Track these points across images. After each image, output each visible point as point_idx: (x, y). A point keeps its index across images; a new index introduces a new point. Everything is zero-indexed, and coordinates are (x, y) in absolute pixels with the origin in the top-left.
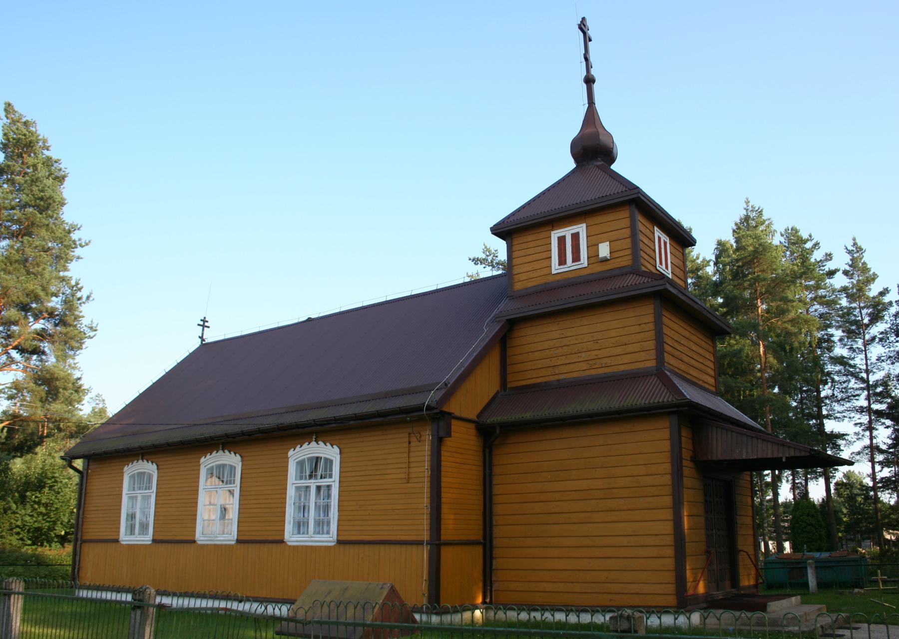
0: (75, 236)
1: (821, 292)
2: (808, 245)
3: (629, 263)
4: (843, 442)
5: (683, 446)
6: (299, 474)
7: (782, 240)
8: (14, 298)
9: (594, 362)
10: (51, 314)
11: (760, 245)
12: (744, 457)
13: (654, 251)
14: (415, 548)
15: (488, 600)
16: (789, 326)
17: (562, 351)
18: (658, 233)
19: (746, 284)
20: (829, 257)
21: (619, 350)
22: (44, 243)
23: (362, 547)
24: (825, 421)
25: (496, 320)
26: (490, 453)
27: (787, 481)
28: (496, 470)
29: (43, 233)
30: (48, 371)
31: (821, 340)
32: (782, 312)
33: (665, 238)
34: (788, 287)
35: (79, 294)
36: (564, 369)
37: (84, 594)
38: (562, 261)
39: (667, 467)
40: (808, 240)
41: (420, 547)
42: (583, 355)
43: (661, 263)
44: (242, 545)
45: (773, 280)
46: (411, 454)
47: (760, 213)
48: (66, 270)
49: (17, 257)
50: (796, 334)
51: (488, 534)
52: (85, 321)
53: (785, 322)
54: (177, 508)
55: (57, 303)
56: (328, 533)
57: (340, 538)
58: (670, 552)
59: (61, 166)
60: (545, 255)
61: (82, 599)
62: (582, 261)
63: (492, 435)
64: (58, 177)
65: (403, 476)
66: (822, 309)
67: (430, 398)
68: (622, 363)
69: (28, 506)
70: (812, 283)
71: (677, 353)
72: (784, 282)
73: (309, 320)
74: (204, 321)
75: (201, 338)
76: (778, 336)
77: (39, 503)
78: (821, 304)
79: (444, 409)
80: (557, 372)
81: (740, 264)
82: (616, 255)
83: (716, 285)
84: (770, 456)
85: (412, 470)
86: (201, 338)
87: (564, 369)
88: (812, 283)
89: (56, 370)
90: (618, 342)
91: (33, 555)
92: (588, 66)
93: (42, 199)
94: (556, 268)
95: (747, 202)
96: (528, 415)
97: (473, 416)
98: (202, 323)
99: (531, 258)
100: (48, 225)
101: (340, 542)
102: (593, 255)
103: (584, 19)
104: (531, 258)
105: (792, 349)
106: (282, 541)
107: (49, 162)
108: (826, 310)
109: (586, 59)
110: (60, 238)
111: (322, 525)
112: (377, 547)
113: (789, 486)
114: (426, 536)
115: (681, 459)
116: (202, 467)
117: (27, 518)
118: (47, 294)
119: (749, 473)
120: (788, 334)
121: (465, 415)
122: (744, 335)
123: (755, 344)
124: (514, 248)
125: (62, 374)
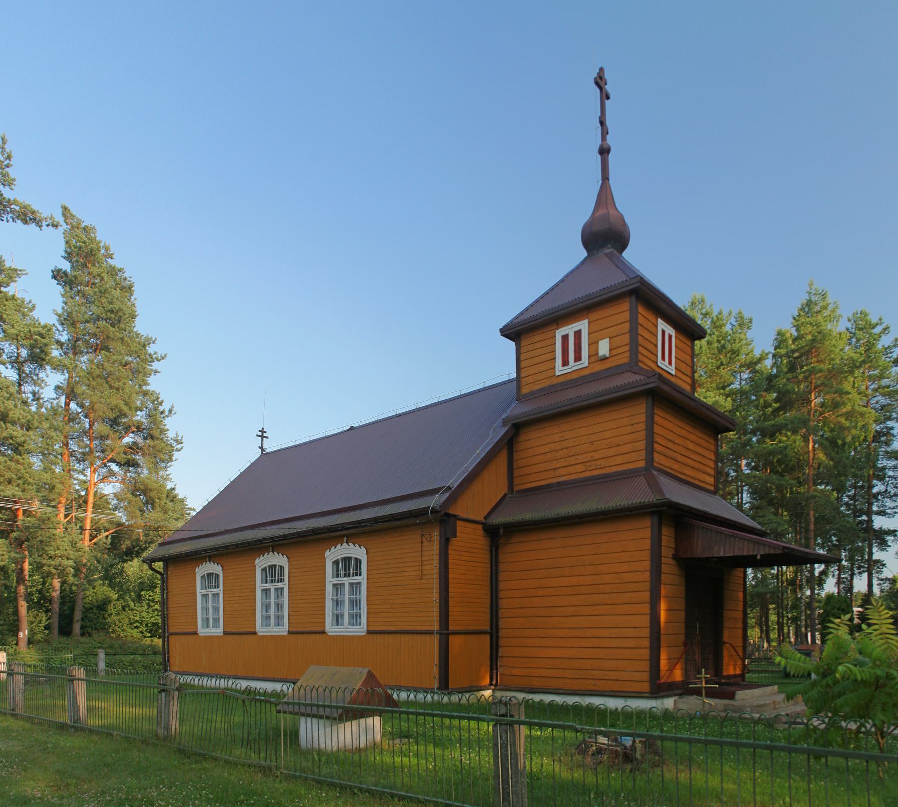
0: (151, 349)
1: (885, 382)
2: (877, 330)
3: (627, 360)
4: (892, 538)
5: (663, 544)
6: (335, 573)
7: (849, 325)
8: (101, 413)
9: (589, 464)
10: (139, 429)
11: (819, 333)
12: (722, 555)
13: (656, 346)
14: (428, 636)
15: (494, 682)
16: (842, 420)
17: (565, 453)
18: (661, 325)
19: (801, 377)
21: (612, 452)
22: (120, 358)
23: (386, 636)
24: (874, 517)
25: (505, 422)
26: (497, 551)
27: (833, 576)
28: (502, 567)
29: (120, 347)
30: (142, 483)
31: (878, 434)
32: (836, 406)
33: (670, 331)
34: (845, 377)
35: (161, 408)
36: (563, 471)
39: (647, 565)
40: (877, 324)
42: (580, 457)
43: (663, 359)
45: (829, 371)
46: (424, 554)
47: (824, 296)
48: (146, 384)
49: (98, 372)
50: (848, 429)
51: (494, 624)
52: (171, 434)
53: (838, 416)
54: (307, 603)
55: (142, 417)
57: (371, 629)
58: (646, 643)
59: (125, 275)
60: (549, 356)
63: (497, 535)
64: (125, 288)
66: (883, 401)
67: (434, 501)
69: (144, 604)
70: (876, 372)
71: (669, 453)
72: (841, 373)
73: (352, 428)
74: (263, 431)
76: (832, 430)
77: (153, 601)
78: (883, 395)
79: (451, 511)
80: (557, 474)
81: (796, 355)
82: (615, 352)
83: (770, 378)
84: (745, 554)
85: (425, 568)
87: (563, 471)
88: (876, 372)
89: (148, 482)
90: (611, 443)
91: (150, 646)
92: (605, 133)
93: (112, 312)
94: (559, 369)
95: (811, 285)
96: (527, 516)
97: (481, 518)
98: (260, 434)
99: (537, 360)
100: (122, 339)
101: (290, 633)
102: (593, 354)
103: (601, 70)
104: (537, 360)
105: (844, 444)
107: (114, 272)
108: (888, 401)
109: (602, 123)
110: (136, 352)
112: (398, 636)
113: (835, 581)
114: (436, 627)
115: (660, 556)
116: (257, 567)
117: (144, 614)
118: (130, 408)
119: (742, 570)
120: (842, 428)
121: (471, 517)
122: (795, 432)
123: (806, 439)
124: (523, 350)
125: (155, 485)
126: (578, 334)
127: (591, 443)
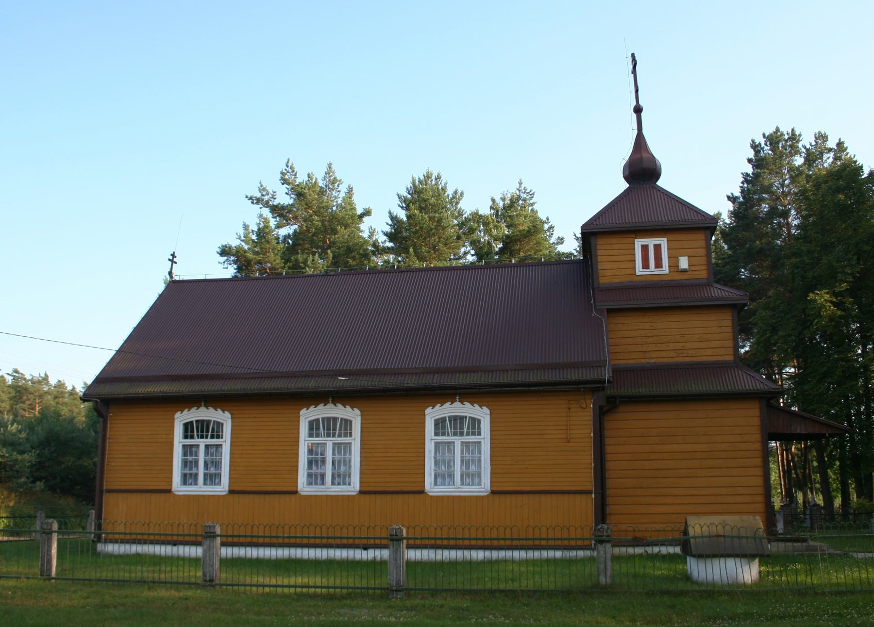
11: (534, 226)
14: (584, 496)
20: (561, 240)
21: (703, 345)
36: (654, 355)
37: (111, 548)
38: (646, 265)
41: (589, 495)
42: (671, 345)
44: (236, 496)
56: (479, 484)
57: (495, 489)
61: (110, 556)
62: (664, 268)
65: (564, 436)
68: (706, 355)
74: (173, 255)
75: (170, 273)
86: (170, 273)
87: (654, 355)
94: (639, 270)
95: (520, 184)
96: (643, 391)
101: (231, 492)
102: (674, 265)
106: (422, 492)
111: (469, 477)
112: (537, 496)
116: (302, 419)
126: (657, 248)
127: (683, 335)
